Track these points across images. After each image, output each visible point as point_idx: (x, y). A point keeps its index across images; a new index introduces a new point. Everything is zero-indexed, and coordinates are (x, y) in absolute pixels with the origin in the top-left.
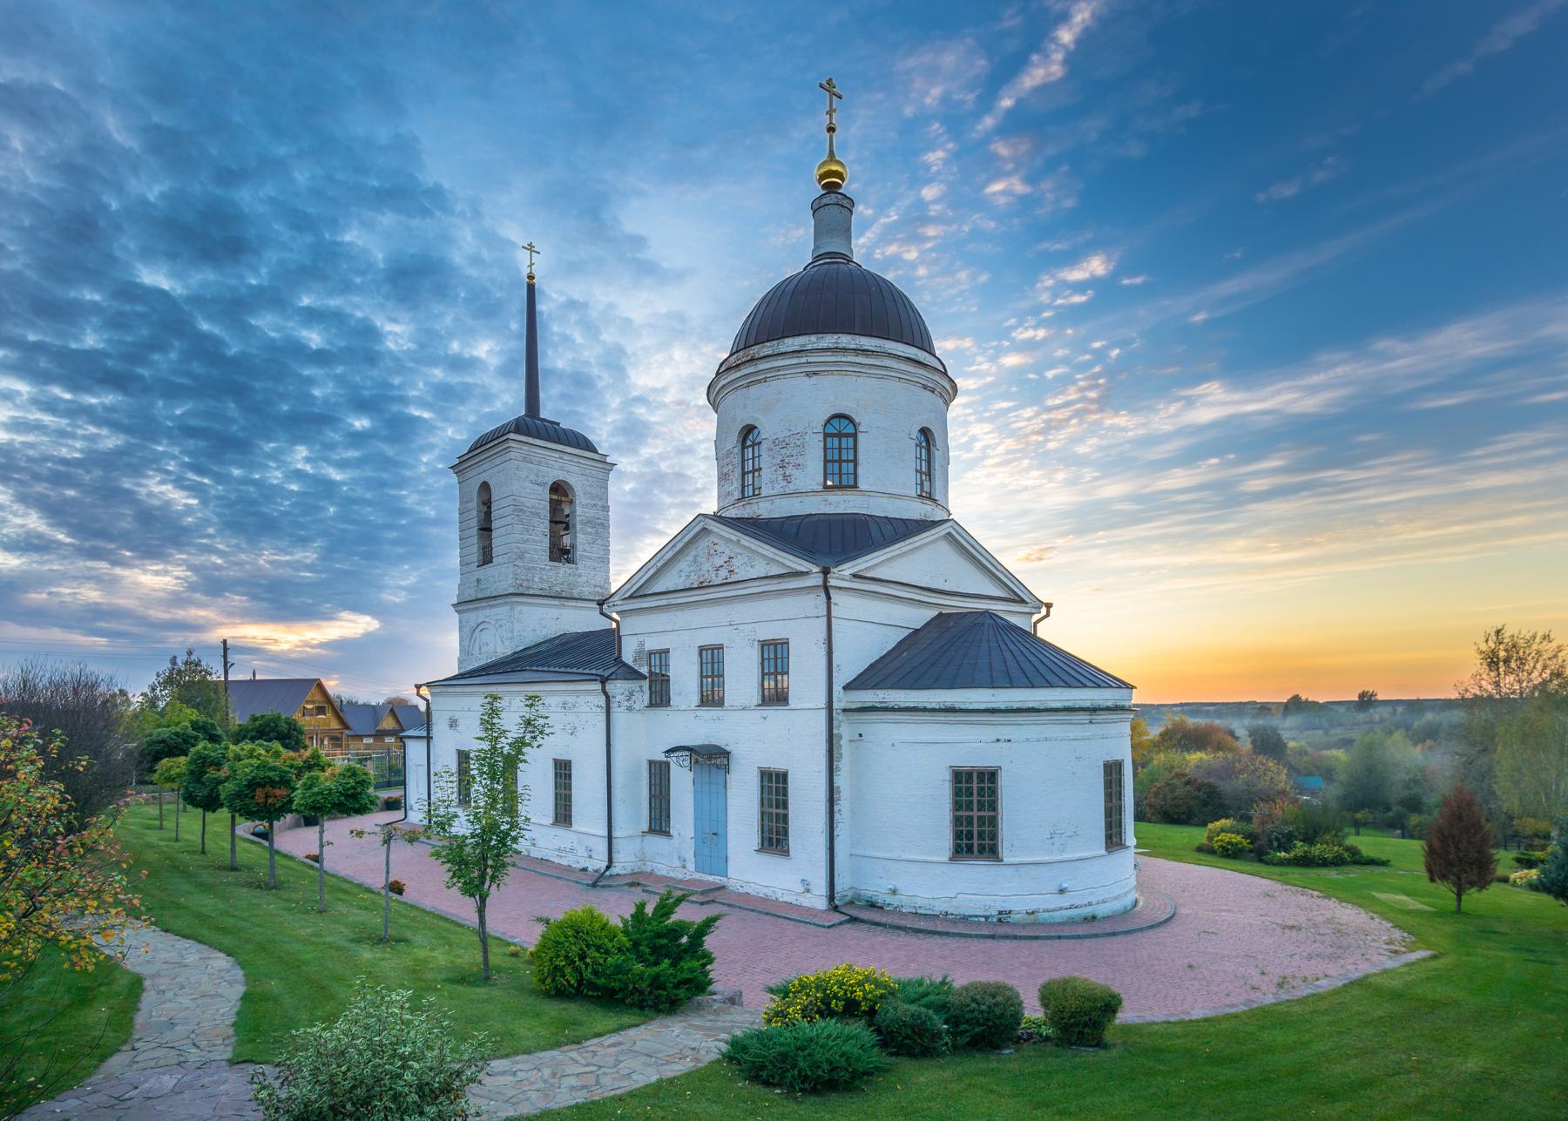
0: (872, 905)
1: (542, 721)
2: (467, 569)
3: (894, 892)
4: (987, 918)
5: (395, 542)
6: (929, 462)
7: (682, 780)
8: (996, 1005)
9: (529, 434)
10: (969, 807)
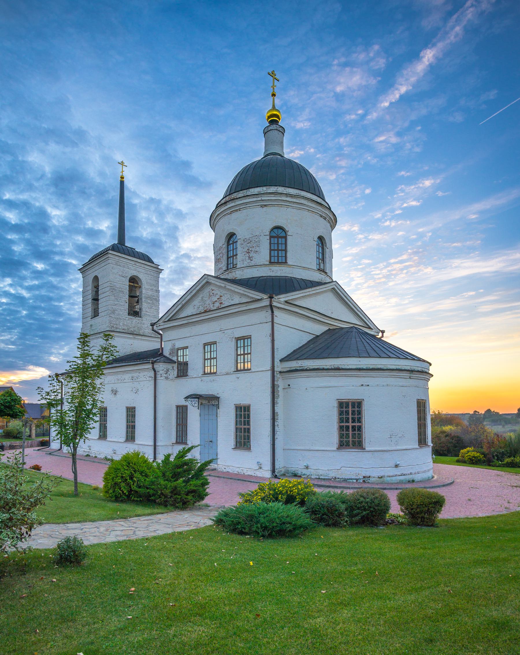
0: (295, 475)
2: (85, 320)
3: (307, 467)
4: (357, 480)
5: (57, 330)
6: (323, 254)
7: (194, 415)
10: (347, 421)
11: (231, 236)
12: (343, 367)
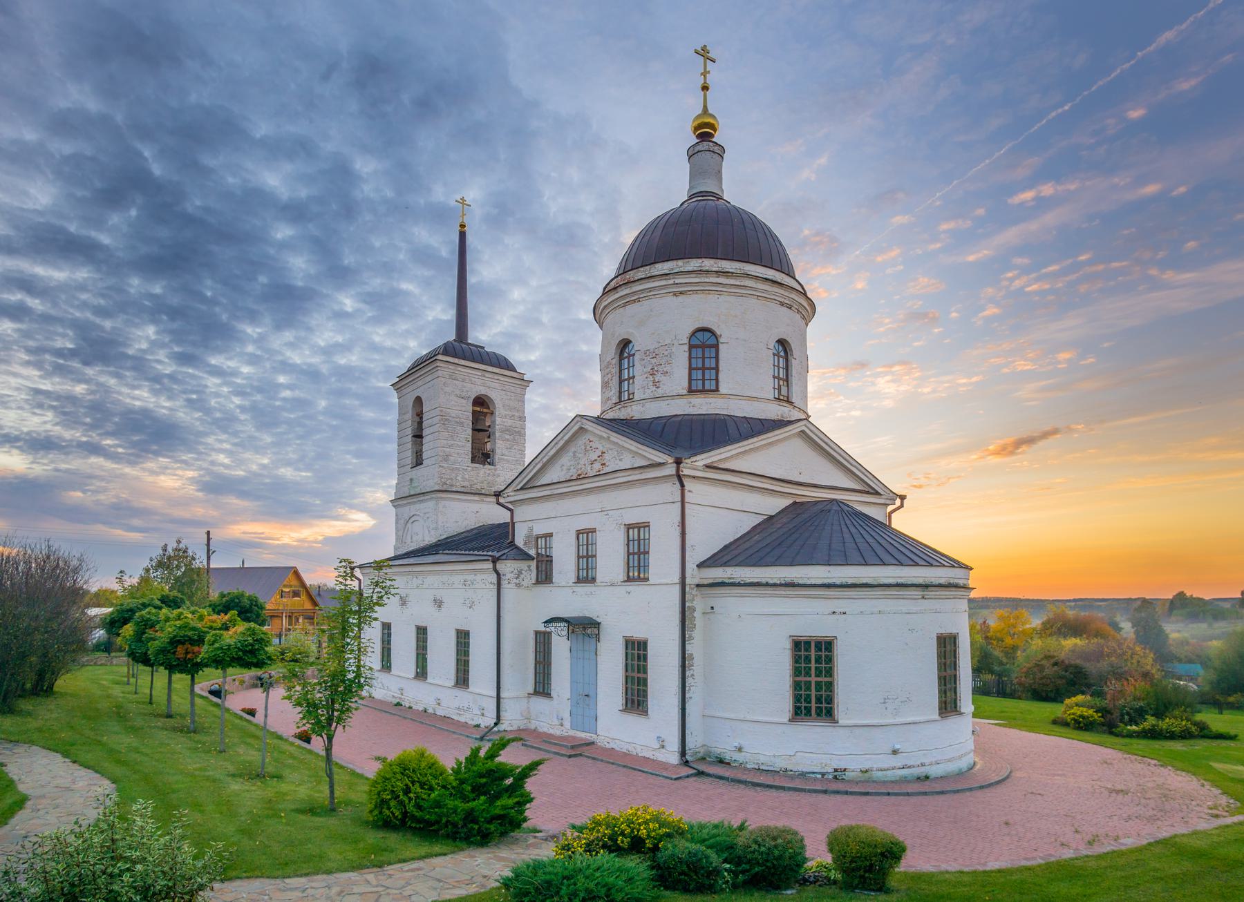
0: (721, 761)
1: (388, 583)
2: (403, 470)
3: (740, 749)
4: (823, 775)
7: (561, 646)
8: (776, 847)
9: (456, 356)
10: (808, 674)
11: (625, 344)
12: (801, 582)
